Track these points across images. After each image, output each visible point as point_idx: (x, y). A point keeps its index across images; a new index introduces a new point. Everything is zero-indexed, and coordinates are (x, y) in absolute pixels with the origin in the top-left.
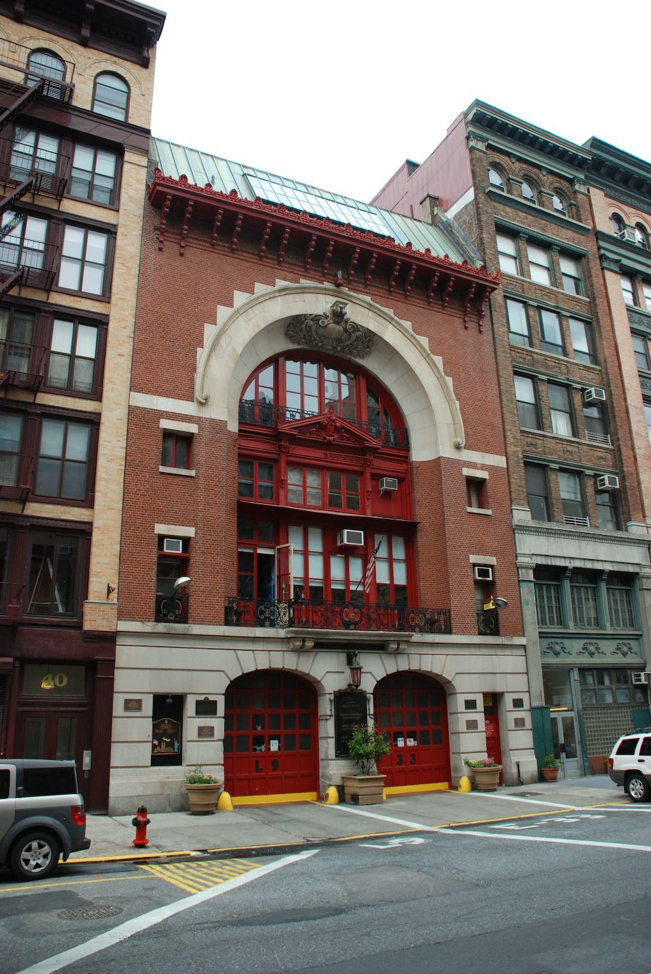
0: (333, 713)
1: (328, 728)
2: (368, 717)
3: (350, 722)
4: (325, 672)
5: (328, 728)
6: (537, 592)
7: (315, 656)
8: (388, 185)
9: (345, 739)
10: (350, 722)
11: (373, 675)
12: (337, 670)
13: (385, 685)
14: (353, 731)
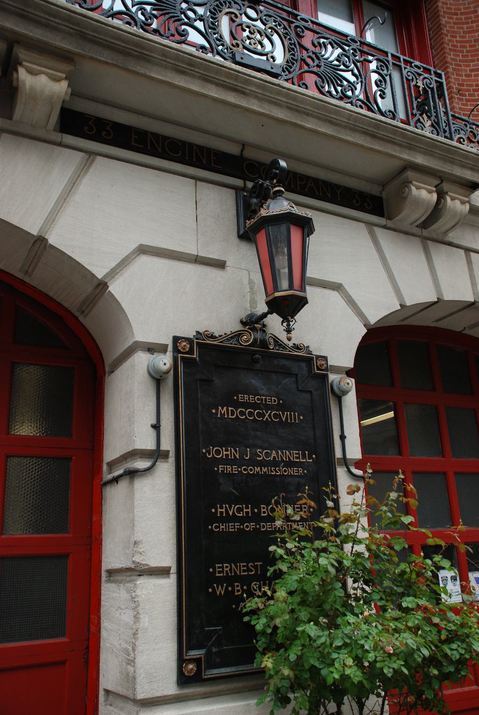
0: (168, 444)
1: (143, 521)
2: (341, 472)
3: (261, 491)
4: (133, 246)
5: (143, 521)
6: (342, 295)
7: (84, 168)
8: (90, 334)
9: (230, 580)
10: (261, 491)
11: (351, 302)
12: (192, 250)
13: (395, 350)
14: (270, 538)
